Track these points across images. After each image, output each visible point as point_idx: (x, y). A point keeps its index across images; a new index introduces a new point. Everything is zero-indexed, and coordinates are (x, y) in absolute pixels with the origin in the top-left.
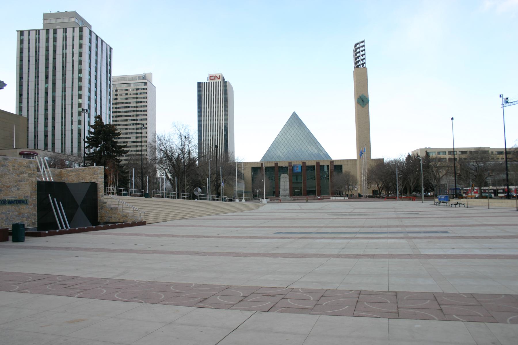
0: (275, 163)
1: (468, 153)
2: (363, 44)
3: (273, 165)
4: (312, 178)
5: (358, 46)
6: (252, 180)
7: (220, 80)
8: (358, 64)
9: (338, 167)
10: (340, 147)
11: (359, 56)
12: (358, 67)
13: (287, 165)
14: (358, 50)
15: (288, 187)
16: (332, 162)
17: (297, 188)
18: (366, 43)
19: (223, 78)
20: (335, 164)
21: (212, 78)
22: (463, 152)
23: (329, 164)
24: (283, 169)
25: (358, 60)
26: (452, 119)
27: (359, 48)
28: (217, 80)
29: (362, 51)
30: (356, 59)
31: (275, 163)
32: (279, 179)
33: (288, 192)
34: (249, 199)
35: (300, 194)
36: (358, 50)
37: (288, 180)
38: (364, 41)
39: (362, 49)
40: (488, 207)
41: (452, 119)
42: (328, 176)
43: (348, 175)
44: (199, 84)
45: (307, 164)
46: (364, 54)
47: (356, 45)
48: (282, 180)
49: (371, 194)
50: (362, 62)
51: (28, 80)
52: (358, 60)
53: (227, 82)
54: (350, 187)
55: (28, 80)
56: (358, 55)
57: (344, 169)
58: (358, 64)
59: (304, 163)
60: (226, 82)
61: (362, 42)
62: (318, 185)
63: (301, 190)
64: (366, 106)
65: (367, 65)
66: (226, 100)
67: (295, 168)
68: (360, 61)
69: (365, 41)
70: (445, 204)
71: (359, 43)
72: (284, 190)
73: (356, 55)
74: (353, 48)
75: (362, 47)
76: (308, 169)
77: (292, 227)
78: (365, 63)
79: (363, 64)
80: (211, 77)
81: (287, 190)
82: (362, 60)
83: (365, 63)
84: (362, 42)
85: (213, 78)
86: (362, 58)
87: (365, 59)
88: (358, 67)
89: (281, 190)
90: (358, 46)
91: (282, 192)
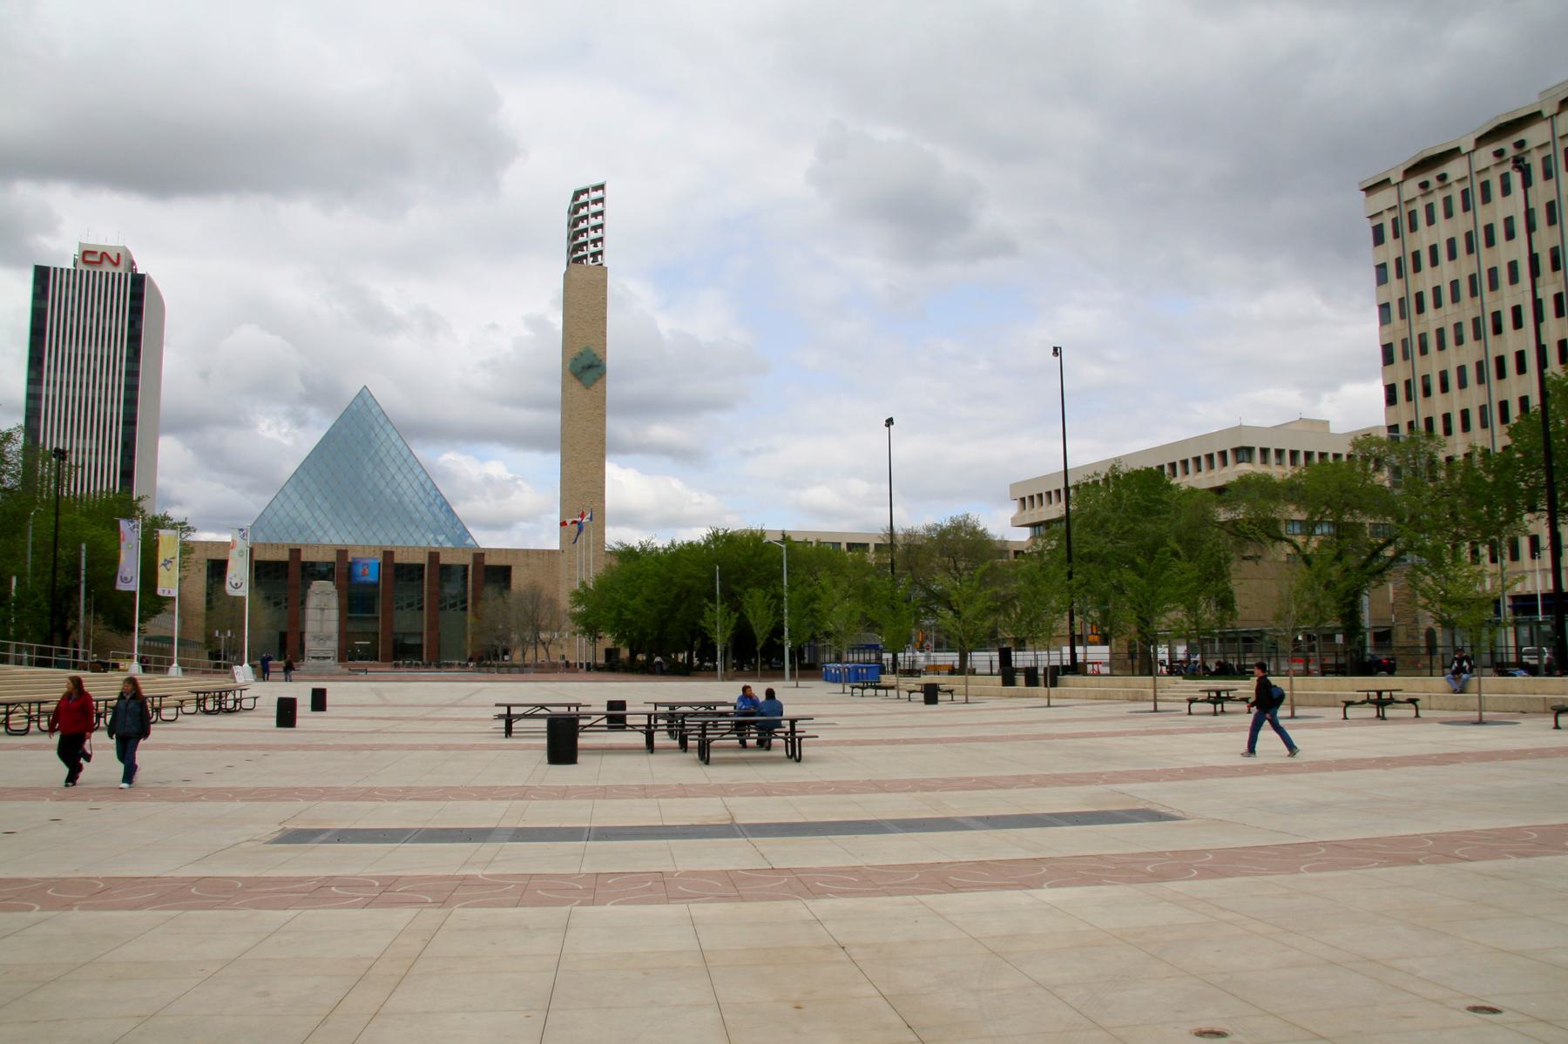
0: (291, 551)
1: (12, 660)
2: (599, 194)
3: (284, 556)
4: (410, 605)
5: (583, 198)
6: (209, 602)
7: (121, 269)
8: (580, 253)
9: (494, 574)
10: (506, 501)
11: (586, 230)
12: (579, 260)
13: (331, 557)
14: (583, 212)
15: (333, 627)
16: (479, 556)
17: (364, 635)
18: (609, 193)
19: (133, 263)
20: (489, 561)
21: (89, 258)
22: (449, 665)
23: (468, 560)
24: (312, 572)
25: (581, 240)
26: (889, 422)
27: (586, 204)
28: (107, 268)
29: (595, 215)
30: (575, 237)
31: (291, 551)
32: (303, 603)
33: (333, 645)
34: (196, 665)
35: (370, 655)
36: (583, 212)
37: (334, 602)
38: (602, 187)
39: (594, 208)
40: (1150, 706)
41: (889, 422)
42: (465, 601)
43: (535, 595)
44: (42, 276)
45: (398, 559)
46: (601, 226)
47: (577, 195)
48: (313, 601)
49: (601, 661)
50: (592, 249)
51: (326, 747)
52: (581, 240)
53: (142, 277)
54: (543, 636)
55: (326, 747)
56: (582, 226)
57: (519, 579)
58: (580, 253)
59: (388, 555)
60: (139, 281)
61: (596, 189)
62: (433, 626)
63: (375, 644)
64: (598, 384)
65: (607, 260)
66: (135, 339)
67: (359, 570)
68: (586, 243)
69: (607, 188)
70: (892, 693)
71: (586, 191)
72: (321, 638)
73: (575, 225)
74: (567, 202)
75: (596, 202)
76: (402, 573)
77: (368, 794)
78: (601, 253)
79: (594, 255)
80: (86, 254)
81: (329, 638)
82: (595, 242)
83: (601, 253)
84: (596, 189)
85: (97, 259)
86: (593, 235)
87: (601, 239)
88: (579, 260)
89: (308, 637)
90: (583, 198)
91: (311, 645)
